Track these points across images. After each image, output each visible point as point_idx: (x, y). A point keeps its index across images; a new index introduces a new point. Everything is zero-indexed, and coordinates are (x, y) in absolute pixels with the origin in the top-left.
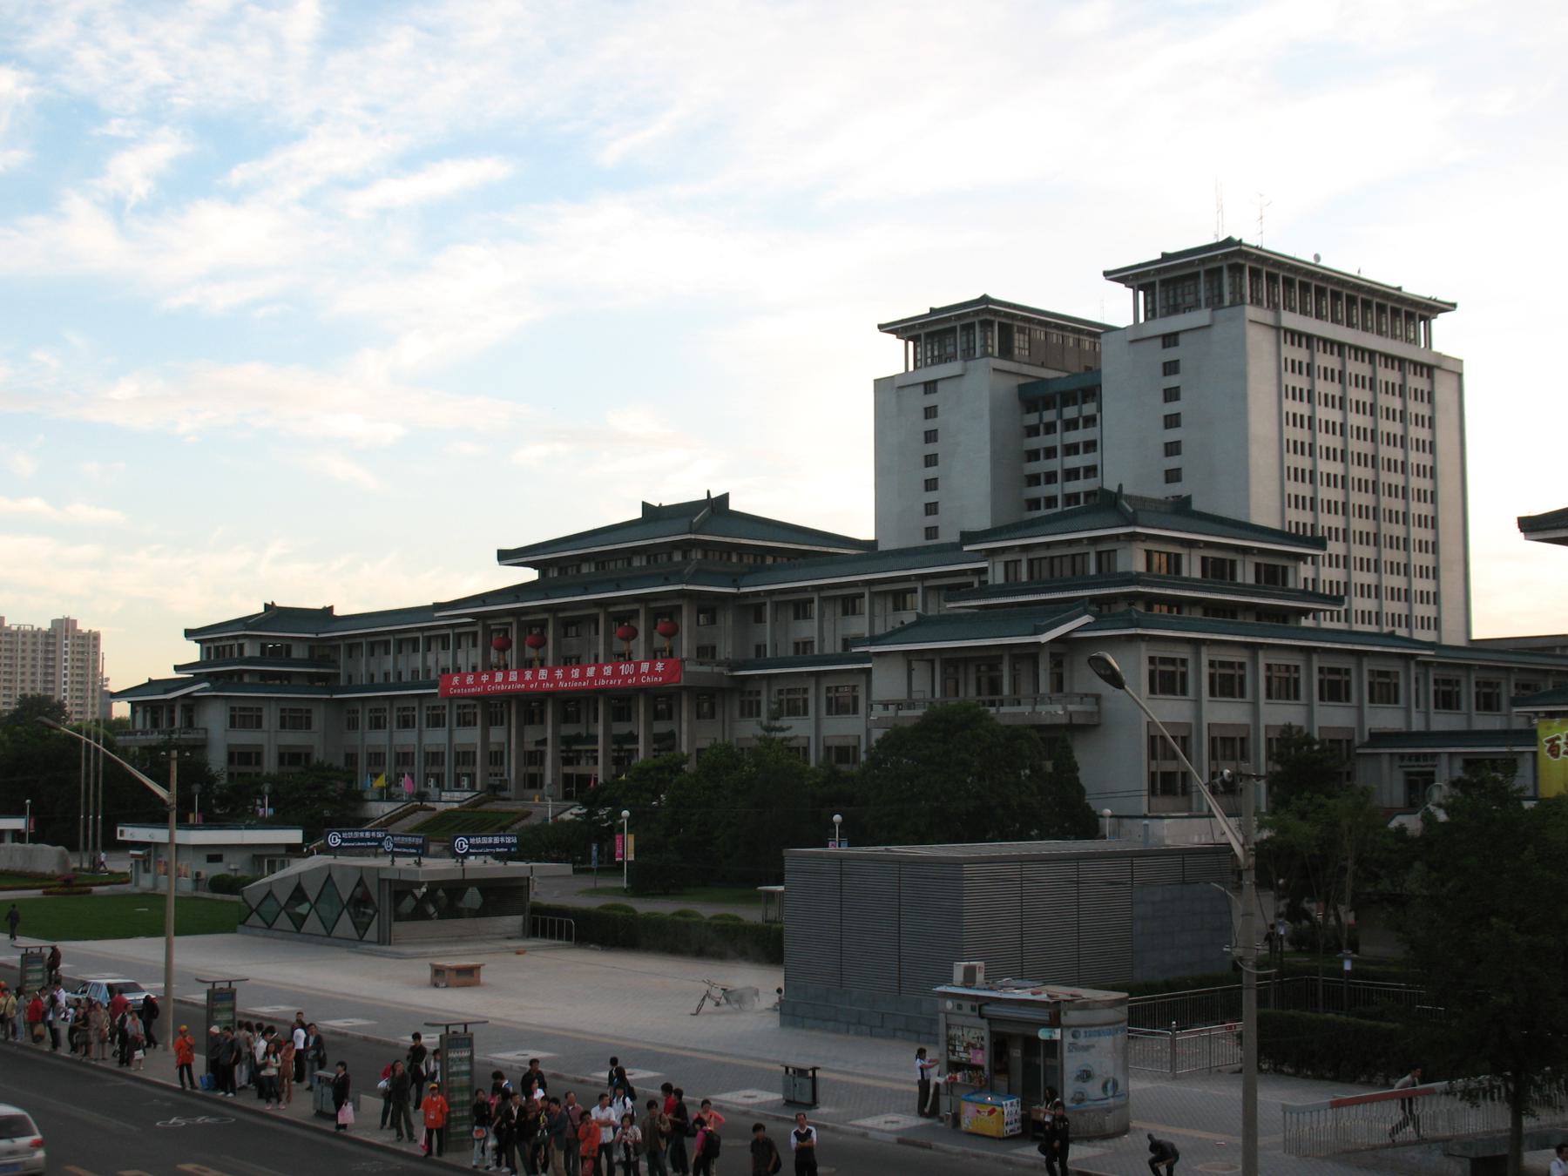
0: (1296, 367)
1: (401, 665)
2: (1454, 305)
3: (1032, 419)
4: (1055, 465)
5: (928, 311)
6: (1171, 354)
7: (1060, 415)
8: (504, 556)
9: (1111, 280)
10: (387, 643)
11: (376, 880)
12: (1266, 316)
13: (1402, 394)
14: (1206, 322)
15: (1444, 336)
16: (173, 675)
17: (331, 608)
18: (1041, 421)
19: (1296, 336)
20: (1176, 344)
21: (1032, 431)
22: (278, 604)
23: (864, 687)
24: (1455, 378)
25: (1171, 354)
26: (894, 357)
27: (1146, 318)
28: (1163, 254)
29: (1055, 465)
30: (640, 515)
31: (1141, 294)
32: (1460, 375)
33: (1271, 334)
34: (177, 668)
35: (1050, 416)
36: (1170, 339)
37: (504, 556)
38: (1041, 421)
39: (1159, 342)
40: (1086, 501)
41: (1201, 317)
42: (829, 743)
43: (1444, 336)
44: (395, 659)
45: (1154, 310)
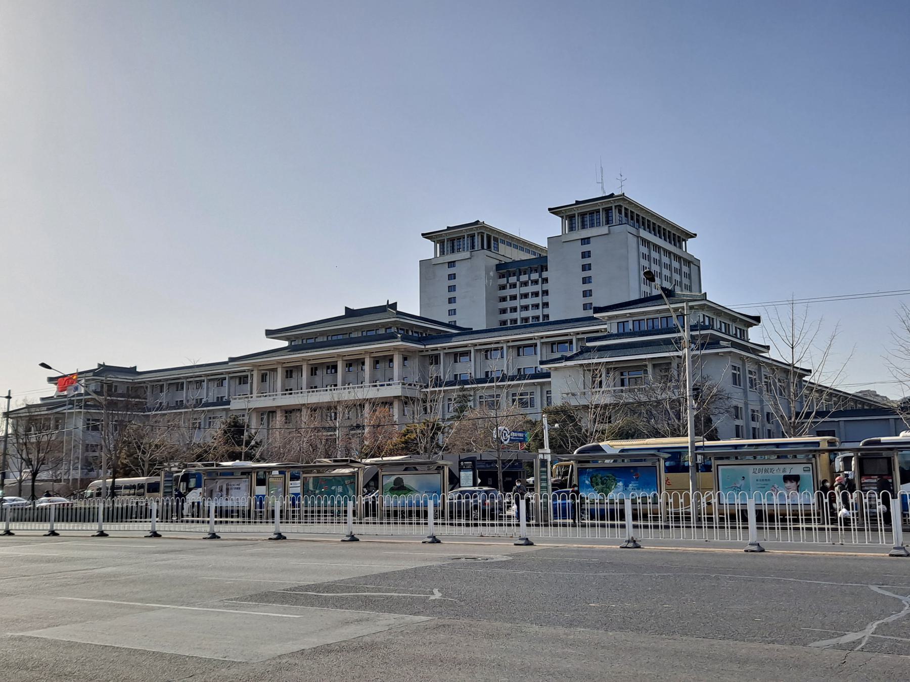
0: (644, 256)
1: (191, 396)
2: (696, 235)
3: (503, 281)
4: (517, 303)
5: (575, 202)
6: (586, 248)
7: (518, 280)
8: (270, 333)
9: (552, 213)
10: (162, 386)
11: (458, 460)
12: (633, 230)
13: (680, 274)
14: (607, 232)
15: (692, 248)
16: (39, 402)
17: (135, 367)
18: (508, 282)
19: (646, 242)
20: (588, 243)
21: (503, 287)
22: (106, 364)
23: (539, 394)
24: (697, 268)
25: (586, 248)
26: (429, 250)
27: (440, 255)
28: (576, 201)
29: (517, 303)
30: (344, 314)
31: (438, 245)
32: (699, 267)
33: (635, 239)
34: (42, 399)
35: (513, 280)
36: (451, 264)
37: (270, 333)
38: (508, 282)
39: (447, 265)
40: (543, 320)
41: (466, 254)
42: (96, 523)
43: (692, 248)
44: (187, 393)
45: (444, 252)
